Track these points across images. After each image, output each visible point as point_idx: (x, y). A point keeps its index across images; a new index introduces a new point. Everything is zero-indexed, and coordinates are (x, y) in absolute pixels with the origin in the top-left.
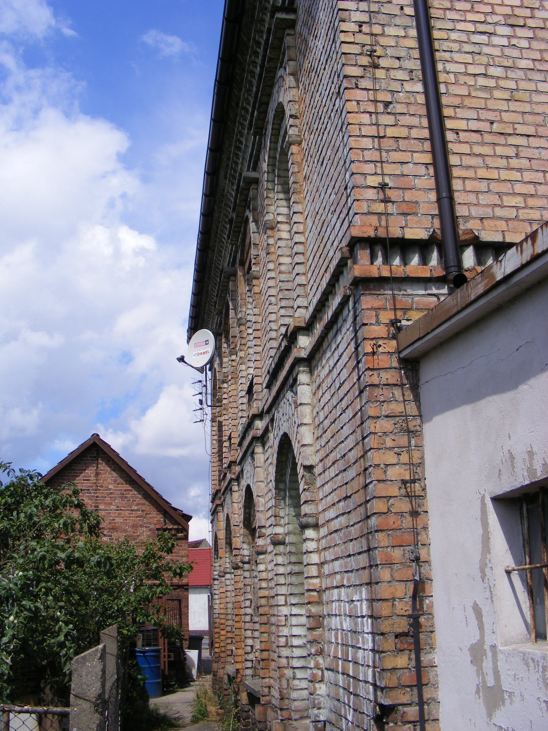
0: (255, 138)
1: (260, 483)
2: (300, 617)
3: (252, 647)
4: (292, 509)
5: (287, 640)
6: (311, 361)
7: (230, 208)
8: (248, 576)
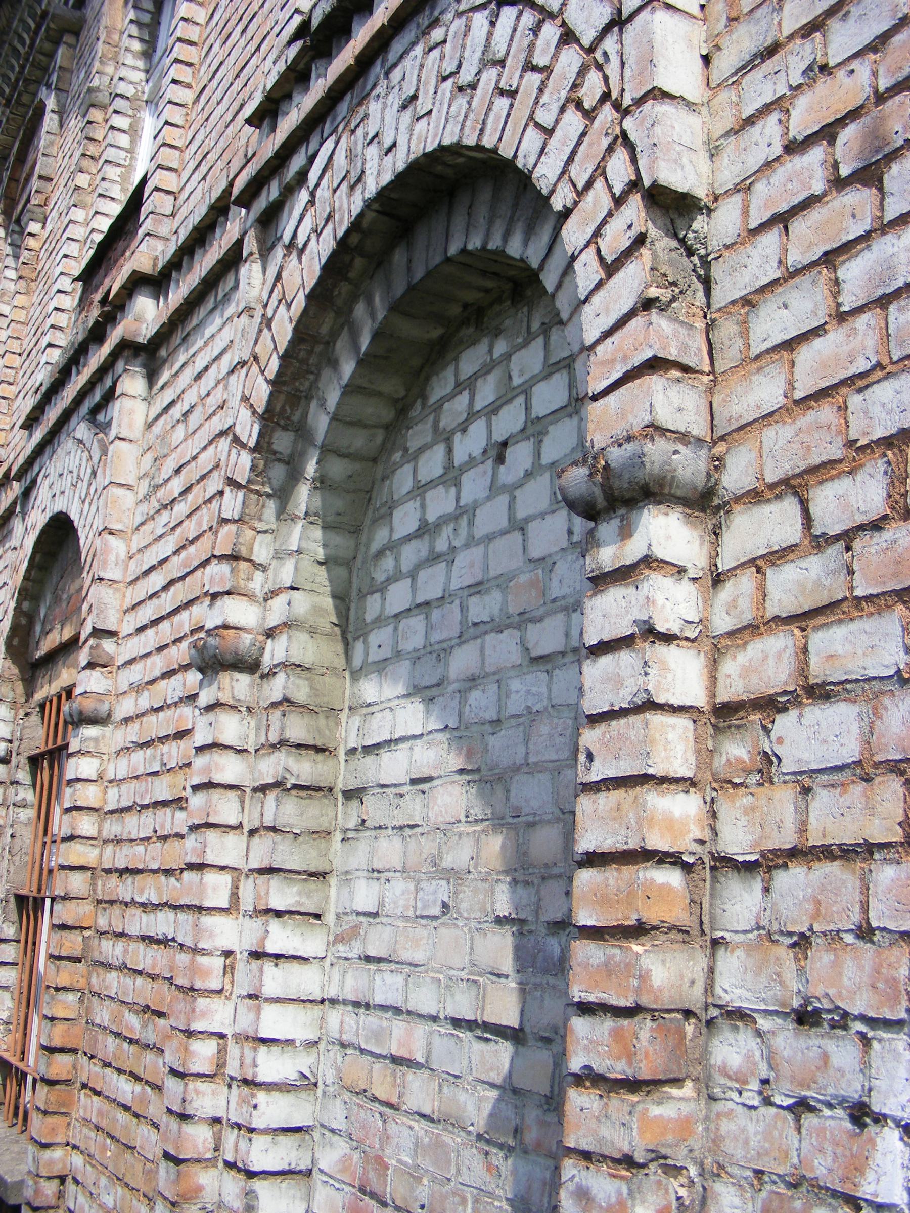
1: (120, 492)
2: (295, 966)
4: (317, 533)
5: (222, 1051)
6: (150, 354)
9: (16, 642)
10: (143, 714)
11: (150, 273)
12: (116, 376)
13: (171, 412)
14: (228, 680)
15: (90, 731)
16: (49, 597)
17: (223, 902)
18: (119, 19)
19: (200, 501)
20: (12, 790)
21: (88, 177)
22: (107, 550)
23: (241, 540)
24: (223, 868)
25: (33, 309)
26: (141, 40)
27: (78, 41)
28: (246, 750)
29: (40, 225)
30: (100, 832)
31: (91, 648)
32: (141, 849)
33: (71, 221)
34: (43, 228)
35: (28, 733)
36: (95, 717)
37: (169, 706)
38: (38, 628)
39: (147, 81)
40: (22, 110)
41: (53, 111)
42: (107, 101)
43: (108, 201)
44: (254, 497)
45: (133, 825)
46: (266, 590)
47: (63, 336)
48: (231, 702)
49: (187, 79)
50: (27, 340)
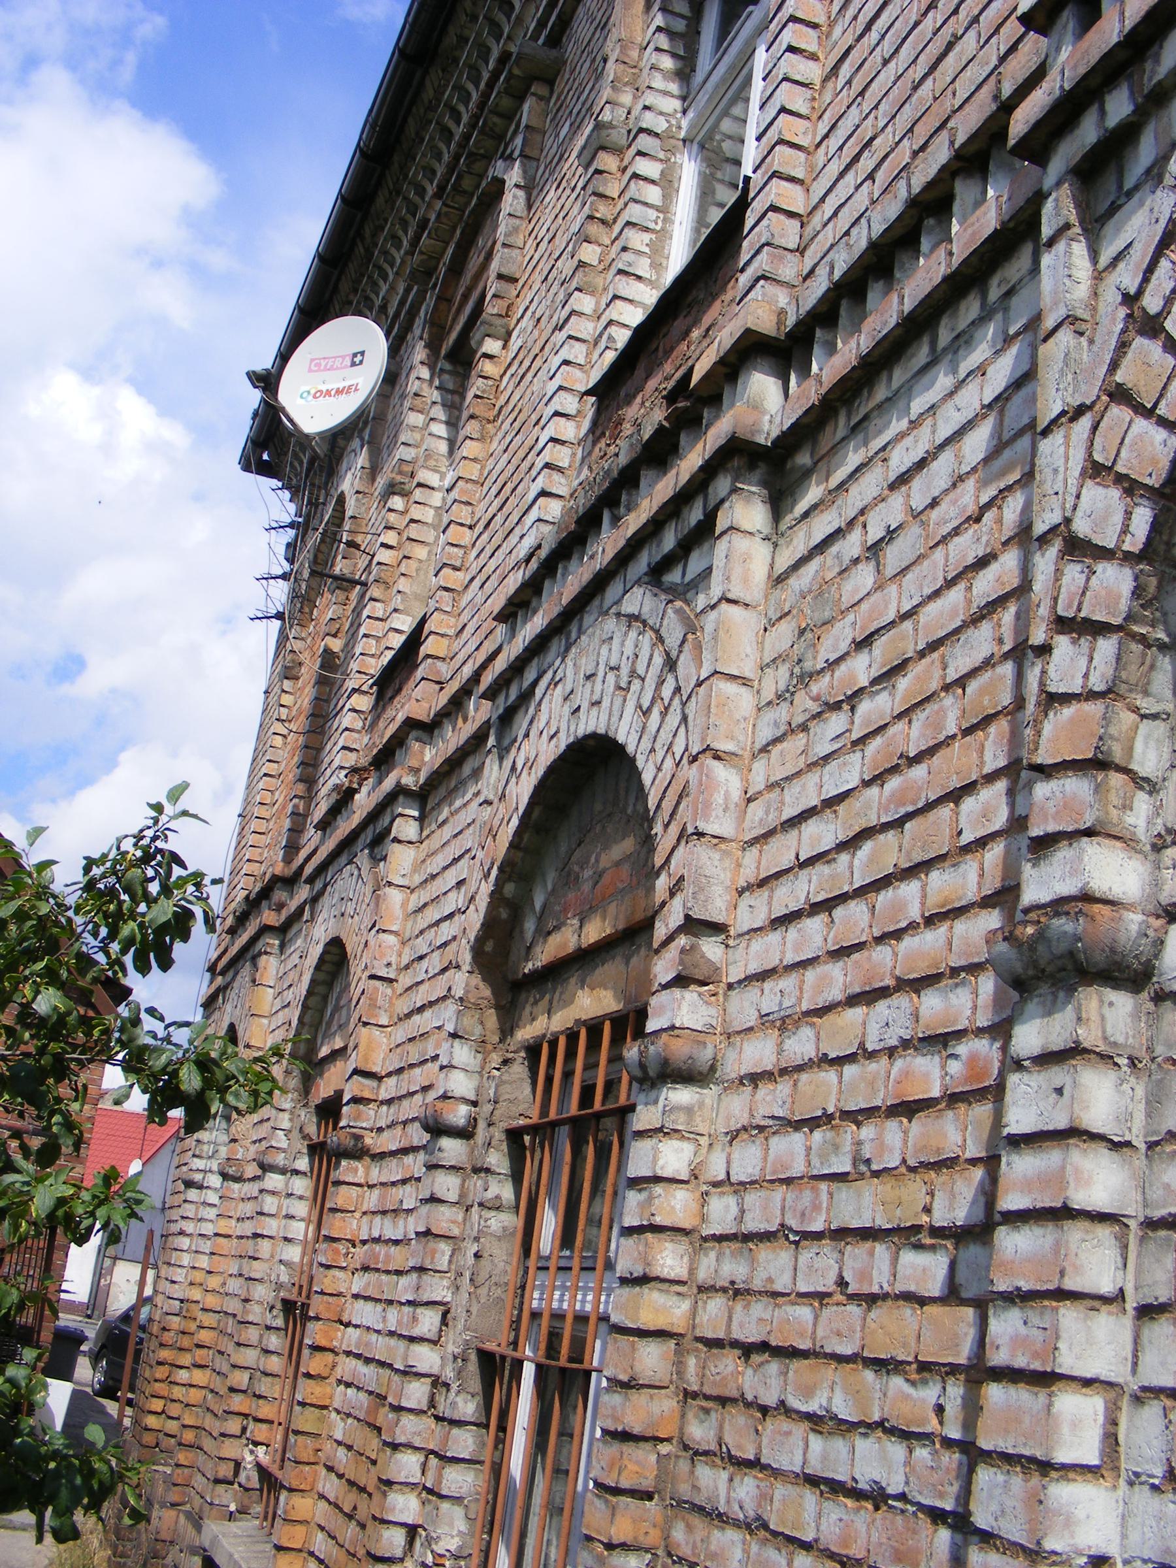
0: (408, 290)
1: (730, 688)
3: (412, 1530)
6: (776, 466)
7: (392, 267)
8: (453, 1196)
9: (489, 947)
10: (800, 1068)
11: (773, 333)
12: (712, 504)
13: (834, 549)
14: (1094, 1004)
15: (681, 1095)
16: (551, 877)
17: (1088, 1451)
18: (639, 28)
19: (934, 685)
20: (476, 1182)
21: (598, 250)
22: (708, 784)
23: (1113, 730)
24: (1088, 1382)
25: (491, 461)
26: (674, 55)
27: (552, 92)
28: (1128, 1144)
29: (500, 343)
30: (692, 1271)
31: (683, 951)
32: (804, 1313)
33: (573, 312)
34: (504, 347)
35: (507, 1092)
36: (690, 1070)
37: (871, 1055)
38: (530, 926)
39: (684, 112)
40: (461, 200)
41: (517, 186)
42: (624, 142)
43: (632, 281)
44: (1137, 648)
45: (775, 1265)
46: (1160, 828)
47: (563, 481)
48: (1102, 1048)
49: (812, 47)
50: (483, 506)
